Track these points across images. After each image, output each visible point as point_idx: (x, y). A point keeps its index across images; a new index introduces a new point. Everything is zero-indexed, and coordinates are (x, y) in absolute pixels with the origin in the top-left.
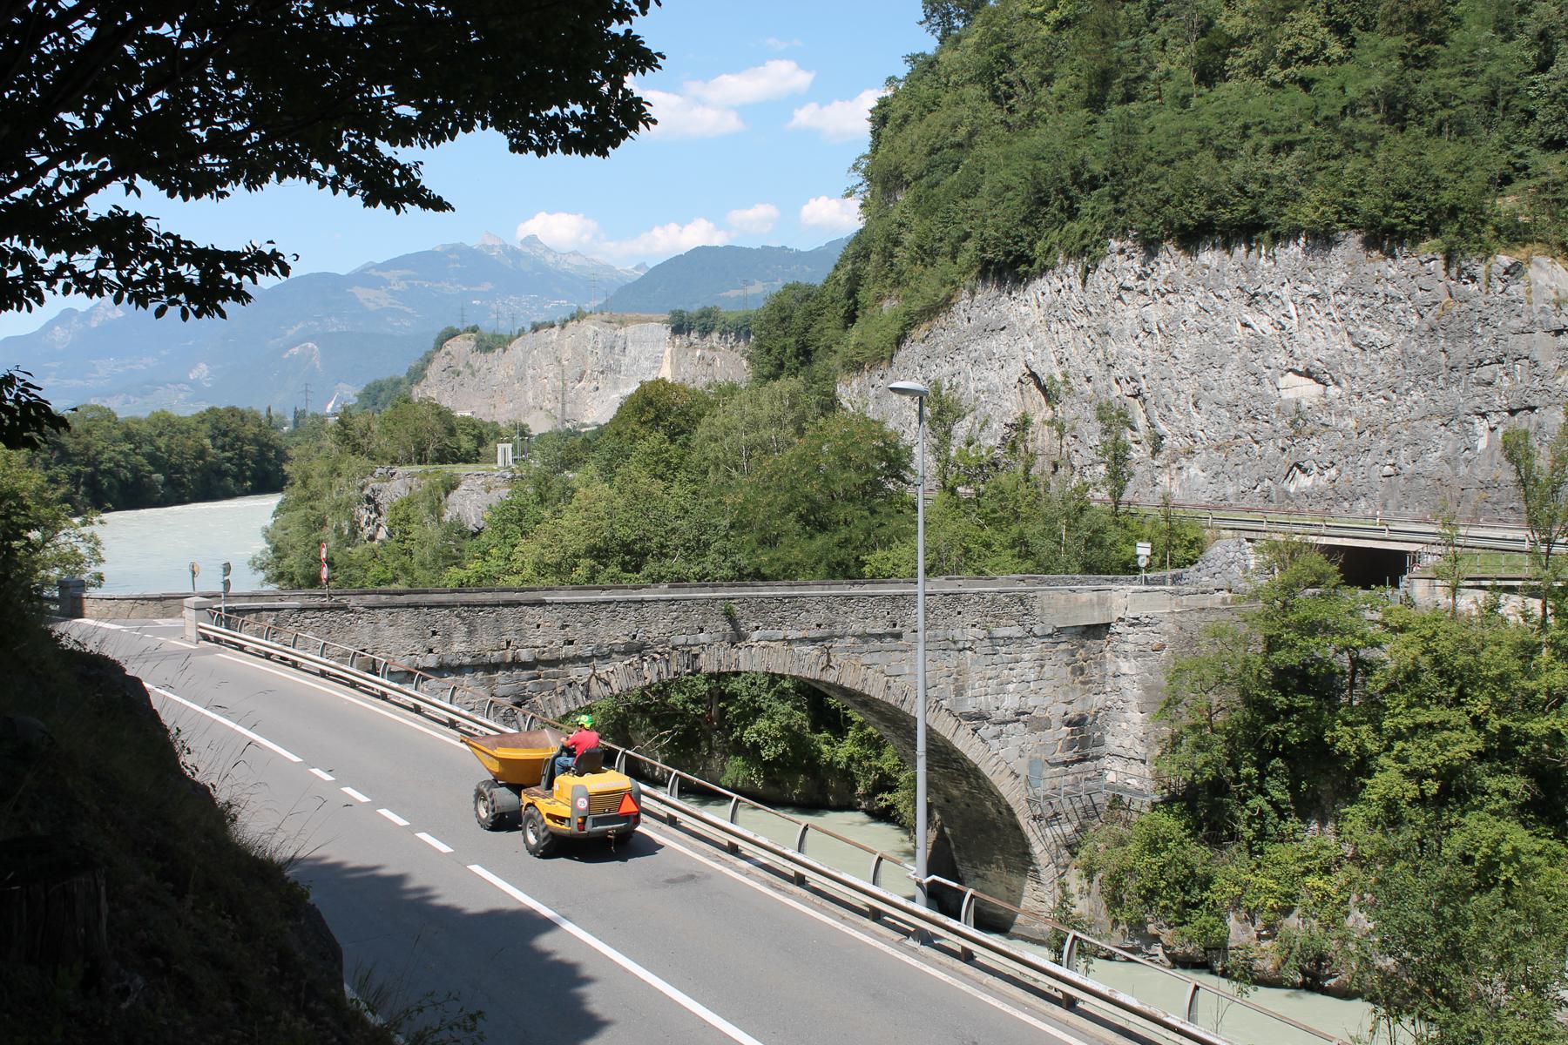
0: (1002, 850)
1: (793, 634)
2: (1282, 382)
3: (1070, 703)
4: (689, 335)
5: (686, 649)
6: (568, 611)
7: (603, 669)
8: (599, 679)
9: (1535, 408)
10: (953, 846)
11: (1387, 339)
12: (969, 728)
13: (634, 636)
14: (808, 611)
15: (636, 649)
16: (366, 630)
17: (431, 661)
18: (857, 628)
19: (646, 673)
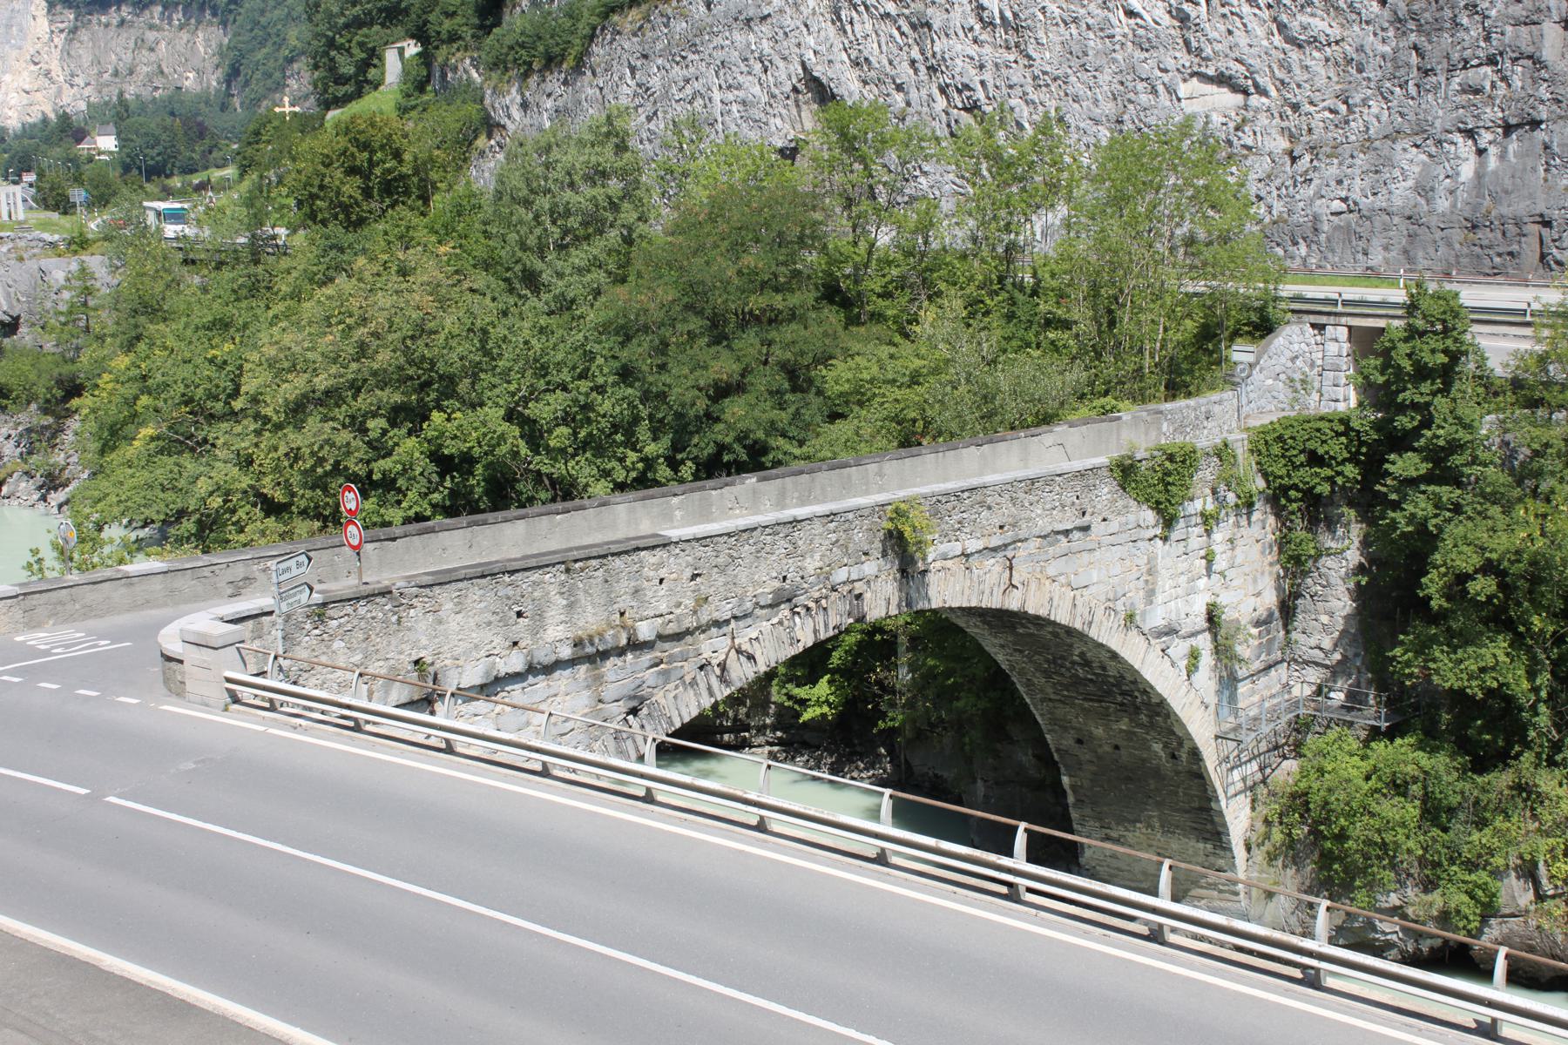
0: (1159, 805)
1: (973, 545)
2: (1183, 90)
3: (1258, 594)
4: (119, 9)
5: (847, 588)
6: (699, 550)
7: (745, 635)
8: (739, 651)
9: (1541, 122)
10: (1071, 799)
11: (1336, 32)
12: (1158, 648)
13: (785, 578)
14: (989, 508)
15: (785, 598)
16: (422, 626)
17: (516, 663)
18: (1044, 524)
19: (799, 634)
